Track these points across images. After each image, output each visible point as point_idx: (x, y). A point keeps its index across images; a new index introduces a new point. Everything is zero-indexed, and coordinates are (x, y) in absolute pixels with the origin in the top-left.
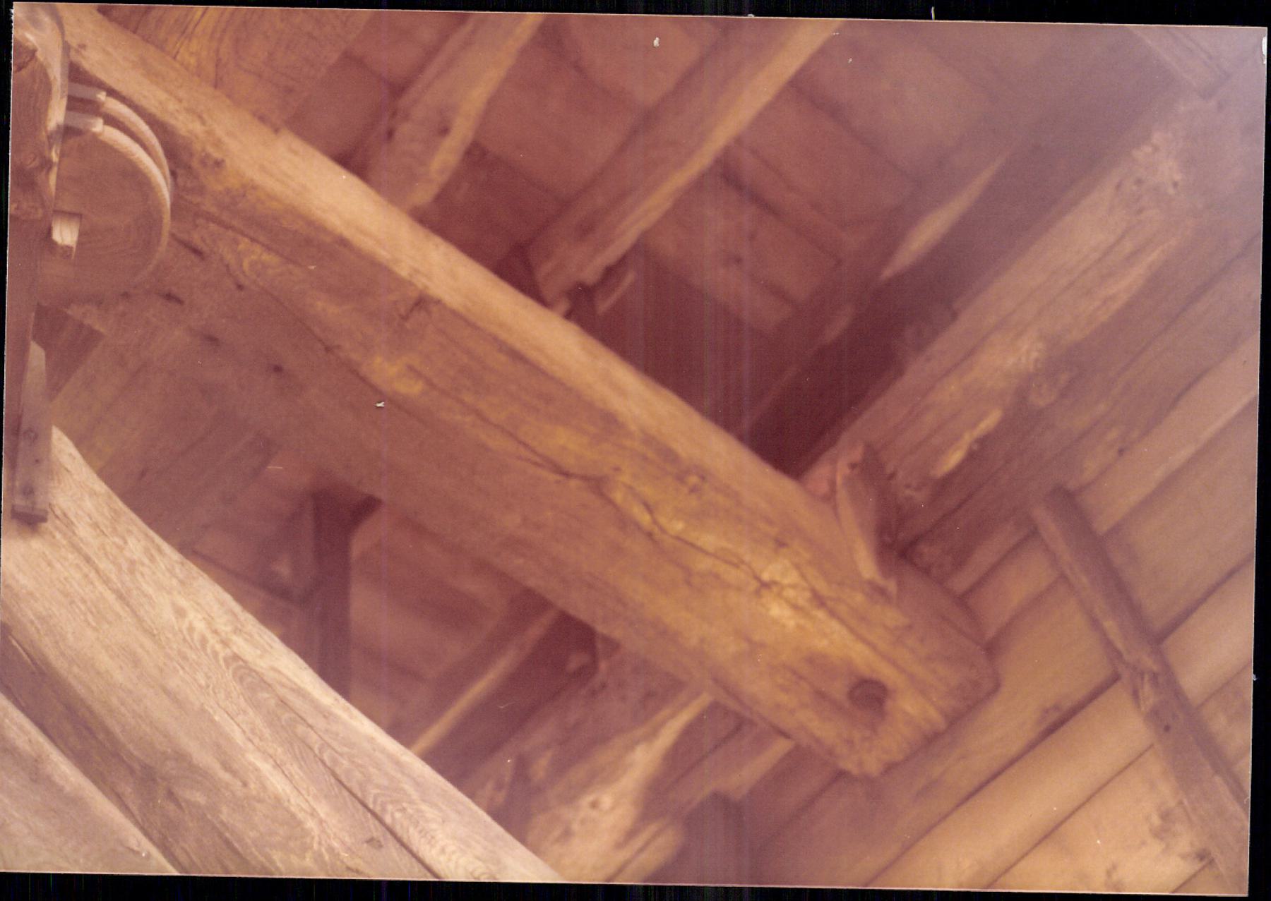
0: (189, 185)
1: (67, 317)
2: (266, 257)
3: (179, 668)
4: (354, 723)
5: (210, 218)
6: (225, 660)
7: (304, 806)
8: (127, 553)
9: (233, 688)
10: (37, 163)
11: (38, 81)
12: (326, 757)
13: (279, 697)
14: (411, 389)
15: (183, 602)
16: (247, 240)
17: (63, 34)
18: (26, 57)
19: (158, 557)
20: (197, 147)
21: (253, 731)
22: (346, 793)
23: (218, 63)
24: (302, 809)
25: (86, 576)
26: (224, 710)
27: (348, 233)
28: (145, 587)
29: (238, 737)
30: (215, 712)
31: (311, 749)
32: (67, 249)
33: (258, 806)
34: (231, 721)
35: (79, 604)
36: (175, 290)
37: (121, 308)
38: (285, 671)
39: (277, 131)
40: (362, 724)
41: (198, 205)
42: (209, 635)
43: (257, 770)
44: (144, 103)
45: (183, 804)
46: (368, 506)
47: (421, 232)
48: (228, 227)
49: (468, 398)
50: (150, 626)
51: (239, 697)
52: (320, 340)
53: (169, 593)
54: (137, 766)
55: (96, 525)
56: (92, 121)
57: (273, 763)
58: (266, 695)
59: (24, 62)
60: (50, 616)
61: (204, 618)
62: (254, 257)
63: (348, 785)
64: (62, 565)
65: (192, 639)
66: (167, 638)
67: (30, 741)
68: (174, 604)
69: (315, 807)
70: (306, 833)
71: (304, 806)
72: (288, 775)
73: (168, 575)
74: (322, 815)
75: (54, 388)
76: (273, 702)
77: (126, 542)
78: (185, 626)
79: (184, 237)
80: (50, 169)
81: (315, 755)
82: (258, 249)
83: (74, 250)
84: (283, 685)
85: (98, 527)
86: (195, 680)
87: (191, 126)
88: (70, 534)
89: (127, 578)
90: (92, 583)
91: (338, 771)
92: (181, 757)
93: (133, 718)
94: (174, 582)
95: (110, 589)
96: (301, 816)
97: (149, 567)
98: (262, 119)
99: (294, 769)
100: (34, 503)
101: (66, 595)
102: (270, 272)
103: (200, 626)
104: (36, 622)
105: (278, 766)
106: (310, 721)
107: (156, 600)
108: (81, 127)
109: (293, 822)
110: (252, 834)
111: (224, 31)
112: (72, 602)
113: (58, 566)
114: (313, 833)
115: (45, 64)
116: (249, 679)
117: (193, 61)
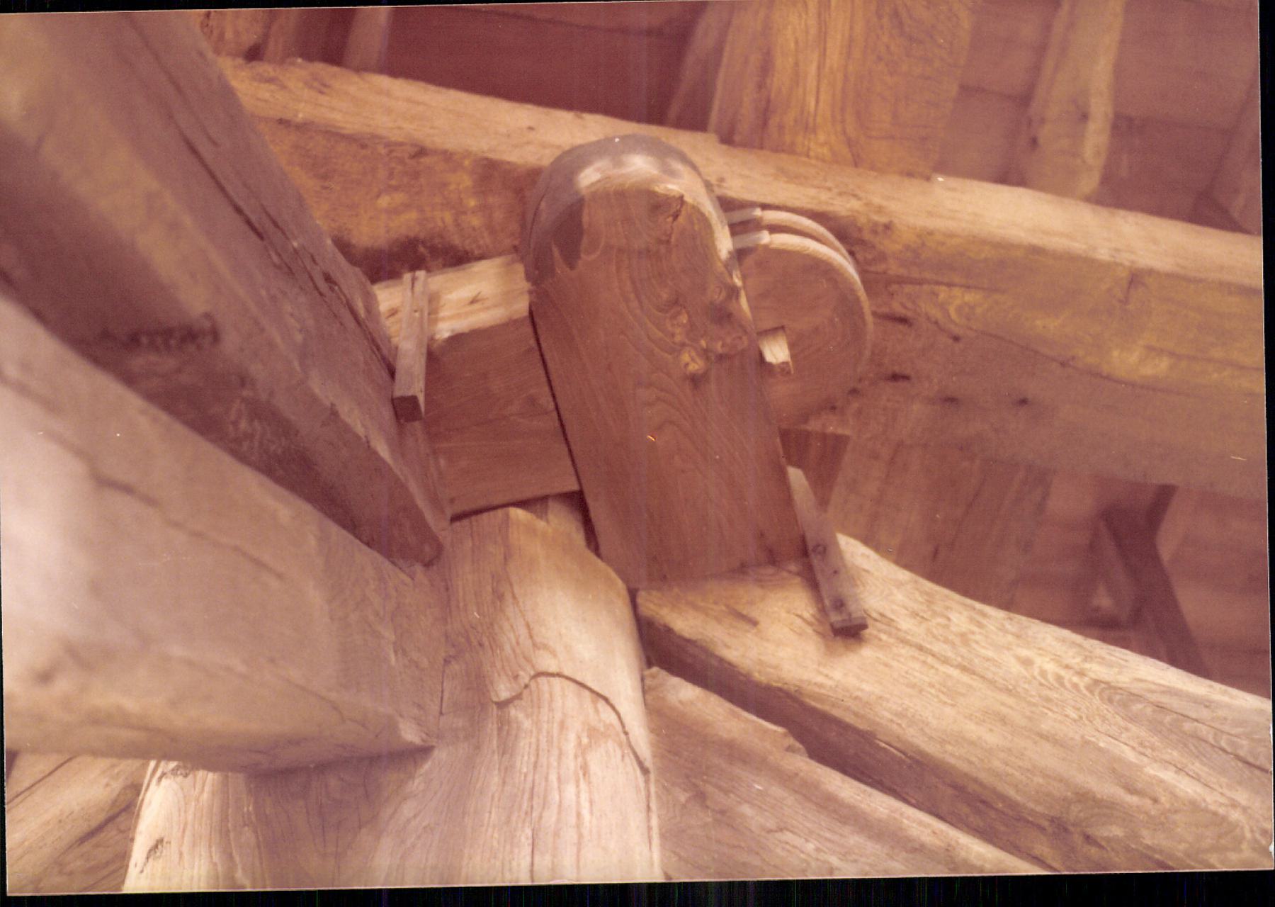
0: (869, 257)
1: (808, 434)
2: (970, 297)
3: (1046, 711)
4: (1236, 702)
5: (901, 281)
6: (1088, 688)
7: (1222, 800)
8: (953, 629)
9: (1105, 712)
10: (724, 294)
11: (696, 221)
12: (1223, 744)
13: (1152, 703)
14: (1160, 367)
15: (1024, 653)
16: (943, 288)
17: (699, 174)
18: (677, 206)
19: (984, 621)
20: (862, 220)
21: (1141, 744)
22: (1257, 772)
23: (850, 143)
24: (1221, 804)
25: (924, 662)
26: (1106, 734)
27: (1036, 240)
28: (983, 652)
29: (1130, 756)
30: (1097, 739)
31: (1206, 742)
32: (783, 367)
33: (1177, 817)
34: (1116, 742)
35: (929, 689)
36: (897, 369)
37: (855, 405)
38: (1150, 678)
39: (928, 179)
40: (1246, 700)
41: (885, 273)
42: (1063, 673)
43: (1161, 781)
44: (797, 204)
45: (1103, 843)
46: (1165, 495)
47: (1104, 212)
48: (920, 282)
49: (1217, 353)
50: (1004, 685)
51: (1115, 718)
52: (1053, 360)
53: (1008, 649)
54: (1046, 824)
55: (915, 614)
56: (757, 236)
57: (1175, 769)
58: (1140, 706)
59: (677, 211)
60: (906, 710)
61: (1052, 659)
62: (958, 302)
63: (1258, 763)
64: (898, 661)
65: (1049, 683)
66: (1024, 689)
67: (934, 833)
68: (1018, 658)
69: (1233, 796)
70: (1233, 826)
71: (1222, 800)
72: (1194, 775)
73: (1000, 634)
74: (1244, 803)
75: (823, 502)
76: (1149, 710)
77: (949, 619)
78: (1036, 673)
79: (885, 310)
80: (738, 297)
81: (1213, 746)
82: (957, 291)
83: (791, 364)
84: (1152, 692)
85: (917, 615)
86: (1066, 716)
87: (848, 206)
88: (894, 631)
89: (963, 650)
90: (933, 667)
91: (1242, 753)
92: (1084, 797)
93: (1022, 774)
94: (1010, 638)
95: (952, 666)
96: (1221, 811)
97: (980, 633)
98: (910, 174)
99: (1197, 767)
100: (850, 614)
101: (913, 686)
102: (979, 310)
103: (1050, 667)
104: (895, 719)
105: (1180, 770)
106: (1194, 715)
107: (1000, 661)
108: (750, 245)
109: (1218, 820)
110: (1182, 846)
111: (843, 110)
112: (921, 691)
113: (895, 664)
114: (1241, 824)
115: (695, 204)
116: (1118, 697)
117: (825, 151)
